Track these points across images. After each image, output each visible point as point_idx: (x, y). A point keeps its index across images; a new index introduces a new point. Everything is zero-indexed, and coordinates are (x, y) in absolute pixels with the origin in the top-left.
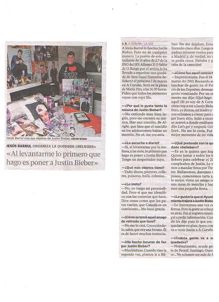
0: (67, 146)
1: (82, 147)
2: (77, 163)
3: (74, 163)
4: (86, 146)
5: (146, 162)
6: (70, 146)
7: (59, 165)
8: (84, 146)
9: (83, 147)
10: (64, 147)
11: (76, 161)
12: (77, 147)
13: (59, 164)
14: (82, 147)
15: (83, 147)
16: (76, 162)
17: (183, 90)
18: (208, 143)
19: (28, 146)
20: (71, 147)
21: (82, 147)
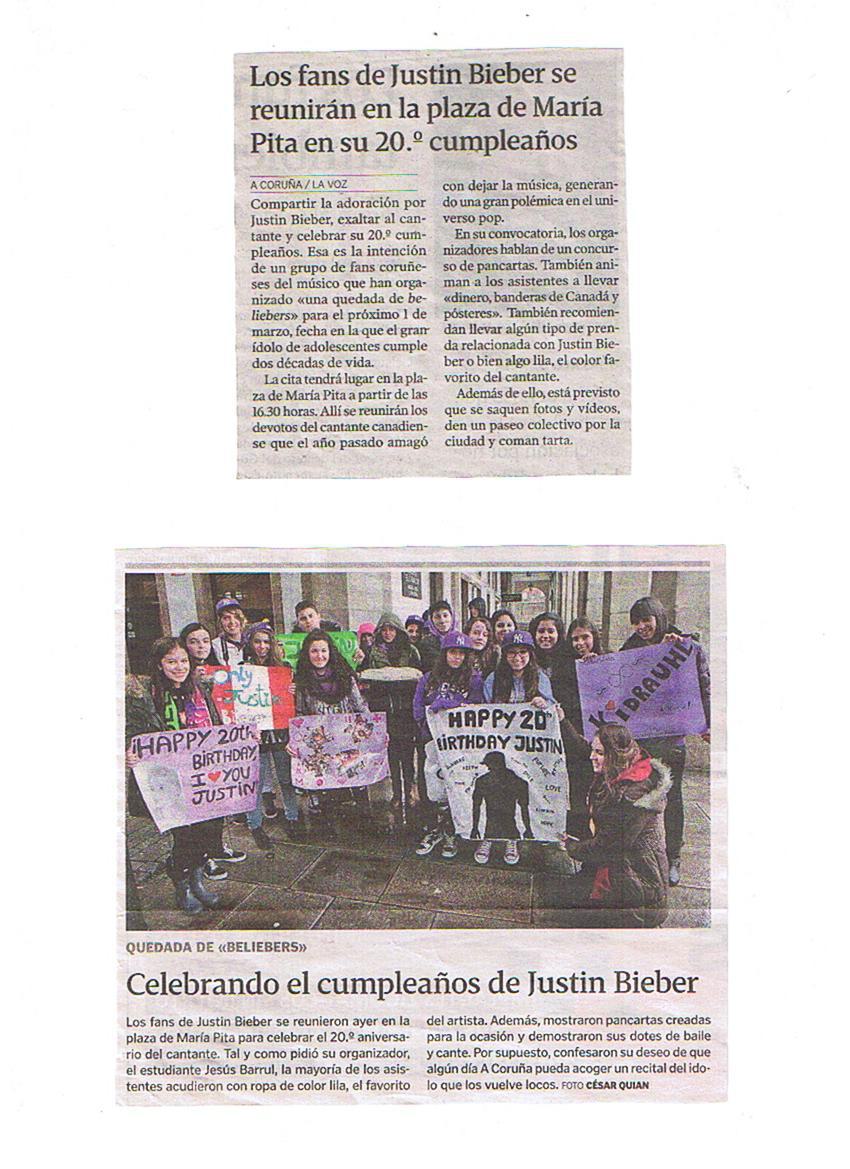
0: (183, 946)
1: (246, 948)
2: (625, 982)
3: (233, 1022)
4: (258, 943)
5: (395, 1096)
6: (175, 944)
7: (494, 992)
8: (254, 943)
9: (250, 947)
10: (153, 949)
11: (618, 977)
12: (226, 949)
13: (546, 987)
14: (243, 949)
15: (250, 947)
16: (621, 980)
17: (576, 234)
18: (340, 1069)
19: (141, 949)
20: (159, 948)
21: (246, 948)
